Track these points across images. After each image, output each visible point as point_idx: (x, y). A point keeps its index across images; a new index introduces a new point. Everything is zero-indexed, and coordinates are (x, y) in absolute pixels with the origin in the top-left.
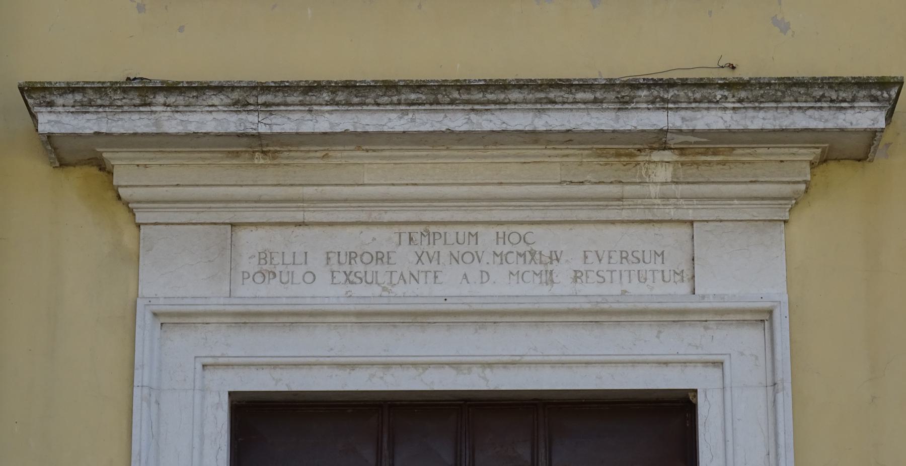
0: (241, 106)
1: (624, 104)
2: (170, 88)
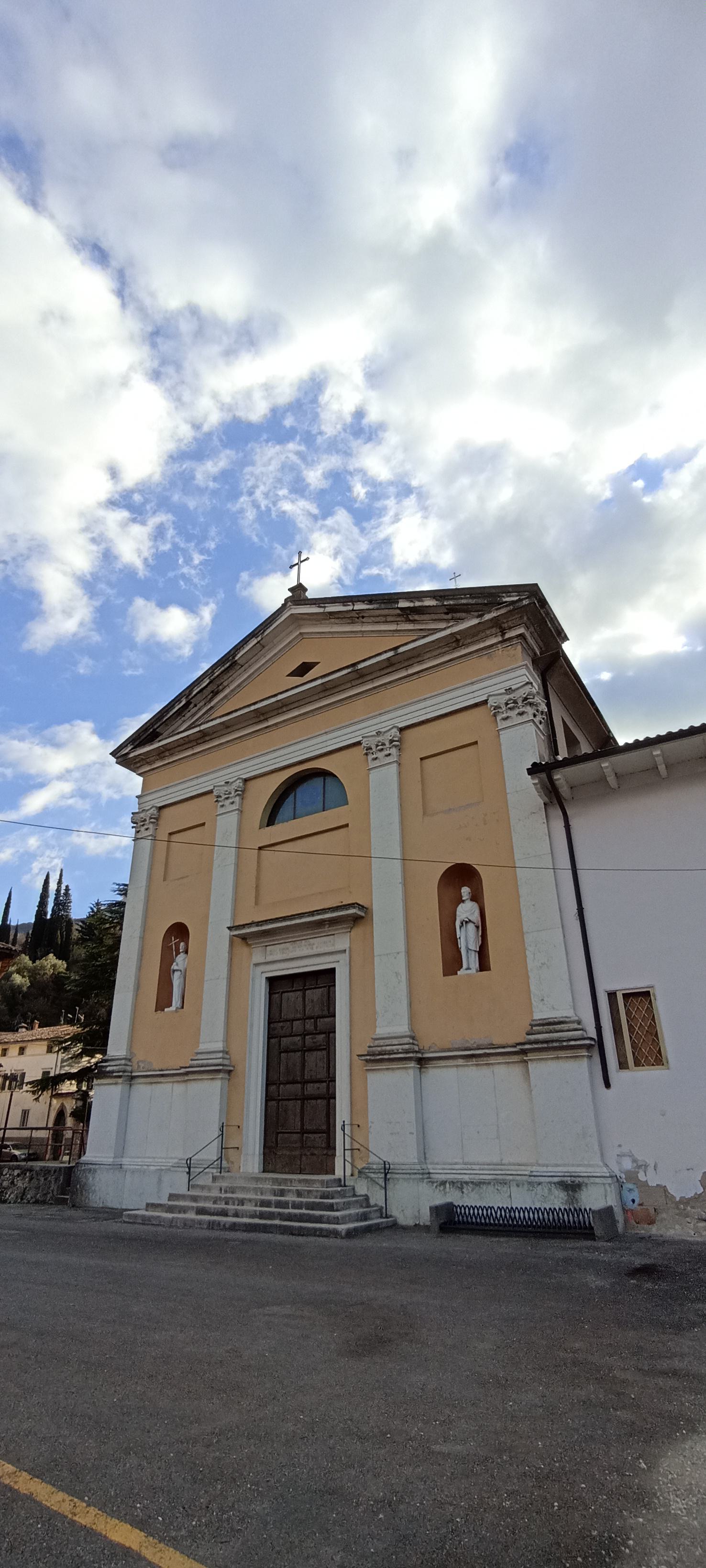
0: (257, 926)
1: (313, 915)
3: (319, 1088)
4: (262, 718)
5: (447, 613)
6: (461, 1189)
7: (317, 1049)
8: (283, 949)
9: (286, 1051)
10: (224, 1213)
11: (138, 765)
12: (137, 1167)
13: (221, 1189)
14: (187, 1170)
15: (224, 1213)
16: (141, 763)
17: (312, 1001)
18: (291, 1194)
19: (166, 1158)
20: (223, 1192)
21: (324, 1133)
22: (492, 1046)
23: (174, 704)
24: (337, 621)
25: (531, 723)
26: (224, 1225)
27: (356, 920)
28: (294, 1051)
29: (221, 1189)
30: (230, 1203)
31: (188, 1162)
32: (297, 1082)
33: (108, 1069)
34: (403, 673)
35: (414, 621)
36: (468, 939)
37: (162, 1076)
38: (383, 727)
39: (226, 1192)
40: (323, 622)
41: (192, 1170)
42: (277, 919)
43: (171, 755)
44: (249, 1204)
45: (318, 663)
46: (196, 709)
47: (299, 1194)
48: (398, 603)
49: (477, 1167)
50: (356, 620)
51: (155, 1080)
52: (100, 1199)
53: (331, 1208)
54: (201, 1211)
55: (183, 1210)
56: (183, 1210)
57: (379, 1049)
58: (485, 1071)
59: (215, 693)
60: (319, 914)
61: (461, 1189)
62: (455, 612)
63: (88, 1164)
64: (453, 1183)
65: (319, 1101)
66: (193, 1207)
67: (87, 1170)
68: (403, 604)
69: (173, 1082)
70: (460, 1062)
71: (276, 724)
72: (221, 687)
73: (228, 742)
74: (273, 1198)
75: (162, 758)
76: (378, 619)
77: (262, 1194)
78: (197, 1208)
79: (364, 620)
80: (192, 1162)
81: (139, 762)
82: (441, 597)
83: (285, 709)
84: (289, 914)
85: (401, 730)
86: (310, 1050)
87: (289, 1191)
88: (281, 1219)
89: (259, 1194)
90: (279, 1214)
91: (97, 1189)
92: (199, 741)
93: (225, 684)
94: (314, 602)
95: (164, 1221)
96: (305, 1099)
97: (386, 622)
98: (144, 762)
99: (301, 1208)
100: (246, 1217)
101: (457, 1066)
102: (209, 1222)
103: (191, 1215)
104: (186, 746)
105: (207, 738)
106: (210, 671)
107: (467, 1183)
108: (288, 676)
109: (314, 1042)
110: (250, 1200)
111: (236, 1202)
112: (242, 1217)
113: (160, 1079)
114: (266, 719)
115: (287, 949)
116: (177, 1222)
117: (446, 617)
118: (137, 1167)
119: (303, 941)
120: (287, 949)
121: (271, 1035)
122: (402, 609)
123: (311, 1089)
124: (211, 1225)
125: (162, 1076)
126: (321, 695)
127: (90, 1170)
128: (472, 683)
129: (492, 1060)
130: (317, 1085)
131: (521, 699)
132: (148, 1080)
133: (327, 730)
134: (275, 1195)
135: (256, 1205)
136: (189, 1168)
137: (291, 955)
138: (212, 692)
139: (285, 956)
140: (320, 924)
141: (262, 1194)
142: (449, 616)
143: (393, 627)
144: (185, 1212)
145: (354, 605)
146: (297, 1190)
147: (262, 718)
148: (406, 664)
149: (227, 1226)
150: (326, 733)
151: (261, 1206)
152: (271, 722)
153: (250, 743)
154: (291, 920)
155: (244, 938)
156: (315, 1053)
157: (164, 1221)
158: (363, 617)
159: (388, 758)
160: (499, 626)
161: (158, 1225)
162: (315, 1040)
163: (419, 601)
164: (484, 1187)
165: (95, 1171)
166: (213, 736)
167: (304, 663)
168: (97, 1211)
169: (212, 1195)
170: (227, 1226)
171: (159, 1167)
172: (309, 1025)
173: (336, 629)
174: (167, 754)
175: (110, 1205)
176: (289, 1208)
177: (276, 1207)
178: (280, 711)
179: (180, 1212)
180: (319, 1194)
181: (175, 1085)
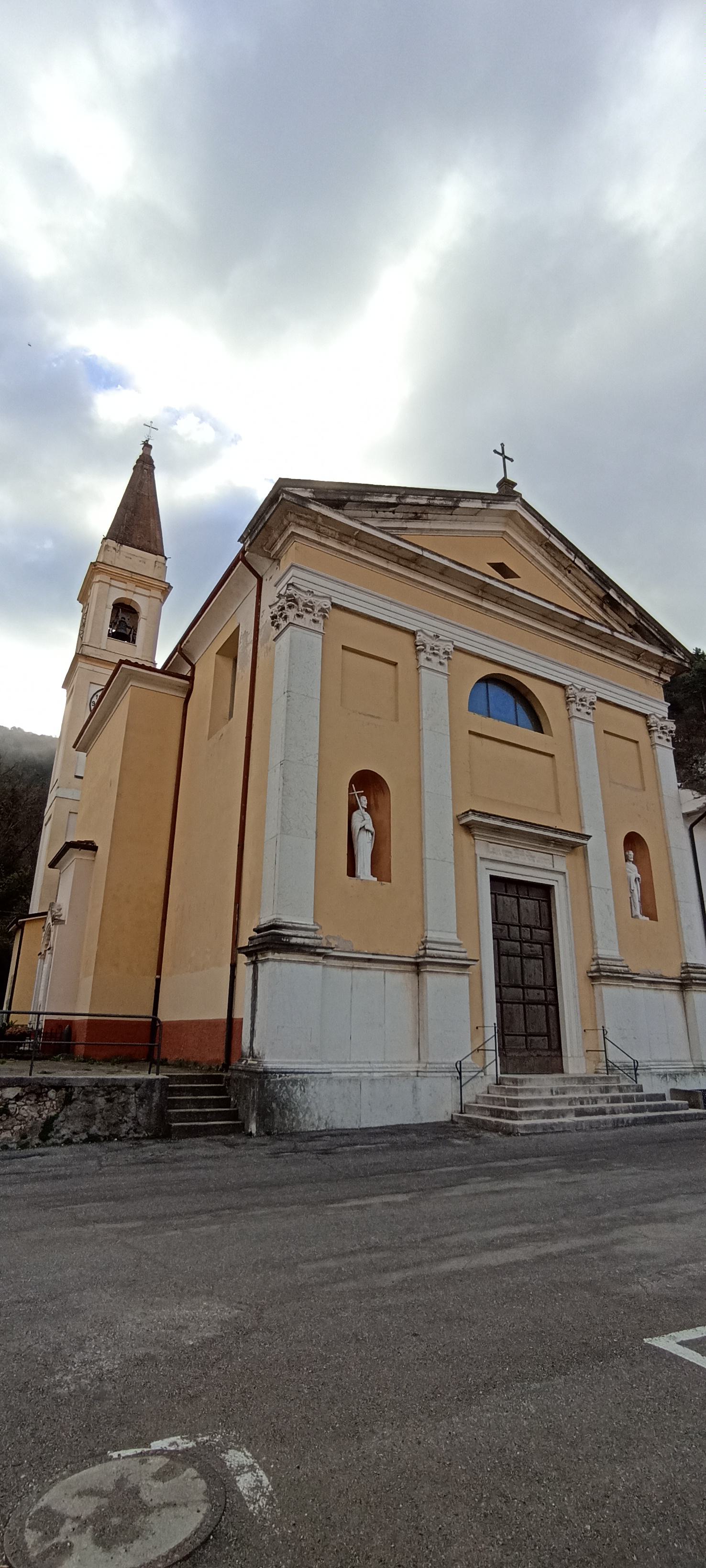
0: (503, 821)
2: (495, 816)
3: (538, 994)
4: (480, 594)
5: (630, 626)
6: (675, 1079)
7: (535, 957)
8: (507, 851)
9: (508, 955)
10: (602, 1112)
11: (303, 522)
12: (352, 1075)
13: (552, 1091)
14: (458, 1075)
15: (602, 1112)
16: (309, 524)
17: (527, 911)
18: (614, 1090)
19: (383, 1062)
20: (554, 1093)
21: (545, 1036)
22: (662, 977)
23: (384, 493)
24: (546, 554)
25: (321, 637)
26: (628, 1121)
27: (573, 846)
28: (514, 956)
29: (552, 1091)
30: (585, 1103)
31: (458, 1066)
32: (518, 987)
33: (294, 940)
34: (597, 649)
35: (605, 611)
36: (365, 845)
37: (369, 960)
38: (589, 688)
39: (557, 1093)
40: (532, 542)
41: (463, 1074)
42: (526, 822)
43: (356, 547)
44: (602, 1101)
45: (518, 577)
46: (391, 515)
47: (620, 1089)
48: (609, 589)
49: (663, 1063)
50: (563, 568)
51: (357, 964)
52: (319, 1119)
53: (516, 1103)
54: (580, 1113)
55: (562, 1114)
56: (562, 1114)
57: (608, 967)
58: (659, 994)
59: (417, 517)
60: (561, 834)
61: (675, 1079)
62: (636, 631)
63: (286, 1073)
64: (670, 1075)
65: (539, 1006)
66: (571, 1110)
67: (288, 1081)
68: (612, 593)
69: (385, 971)
70: (645, 985)
71: (487, 610)
72: (424, 516)
73: (432, 587)
74: (600, 1095)
75: (341, 541)
76: (580, 585)
77: (590, 1092)
78: (576, 1110)
79: (569, 575)
80: (462, 1066)
81: (307, 520)
82: (641, 614)
83: (504, 603)
84: (524, 820)
85: (334, 605)
86: (530, 957)
87: (612, 1087)
88: (649, 1111)
89: (588, 1092)
90: (648, 1106)
91: (313, 1106)
92: (402, 562)
93: (430, 516)
94: (544, 522)
95: (569, 1127)
96: (526, 1003)
97: (584, 592)
98: (314, 527)
99: (643, 1101)
100: (622, 1113)
101: (644, 988)
102: (614, 1120)
103: (570, 1119)
104: (383, 554)
105: (413, 566)
106: (433, 494)
107: (678, 1074)
108: (489, 564)
109: (532, 951)
110: (602, 1098)
111: (590, 1102)
112: (618, 1113)
113: (367, 965)
114: (482, 598)
115: (511, 852)
116: (582, 1125)
117: (627, 628)
118: (352, 1075)
119: (525, 851)
120: (511, 852)
121: (550, 942)
122: (608, 595)
123: (532, 994)
124: (591, 1125)
125: (369, 960)
126: (568, 629)
127: (295, 1082)
128: (640, 695)
129: (662, 986)
130: (537, 991)
131: (319, 608)
132: (349, 964)
133: (642, 693)
134: (602, 1092)
135: (608, 1102)
136: (460, 1073)
137: (515, 861)
138: (416, 513)
139: (507, 860)
140: (547, 840)
141: (590, 1092)
142: (630, 630)
143: (588, 601)
144: (564, 1116)
145: (575, 558)
146: (619, 1086)
147: (480, 594)
148: (604, 645)
149: (630, 1122)
150: (391, 602)
151: (612, 1102)
152: (485, 604)
153: (456, 607)
154: (545, 830)
155: (468, 828)
156: (532, 961)
157: (569, 1127)
158: (570, 572)
159: (586, 715)
160: (663, 664)
161: (563, 1132)
162: (532, 949)
163: (624, 602)
164: (687, 1076)
165: (304, 1082)
166: (422, 570)
167: (503, 564)
168: (317, 1136)
169: (544, 1097)
170: (630, 1122)
171: (386, 1074)
172: (526, 934)
173: (539, 557)
174: (353, 542)
175: (339, 1125)
176: (633, 1102)
177: (624, 1102)
178: (500, 601)
179: (558, 1117)
180: (635, 1088)
181: (388, 974)
